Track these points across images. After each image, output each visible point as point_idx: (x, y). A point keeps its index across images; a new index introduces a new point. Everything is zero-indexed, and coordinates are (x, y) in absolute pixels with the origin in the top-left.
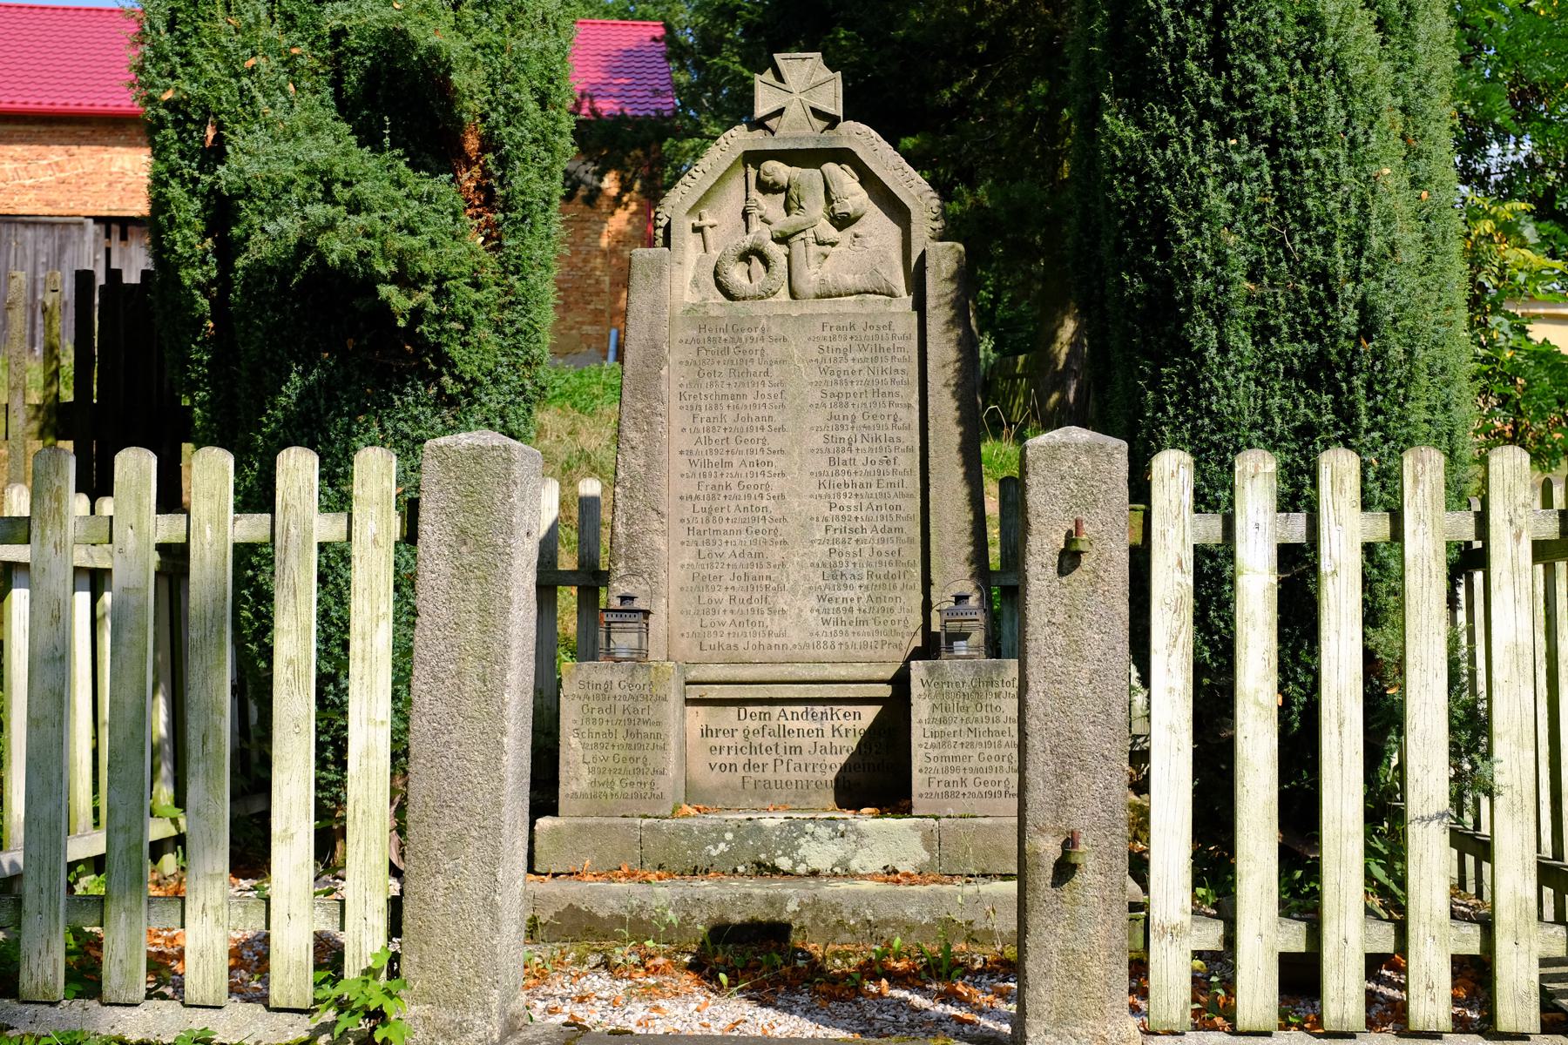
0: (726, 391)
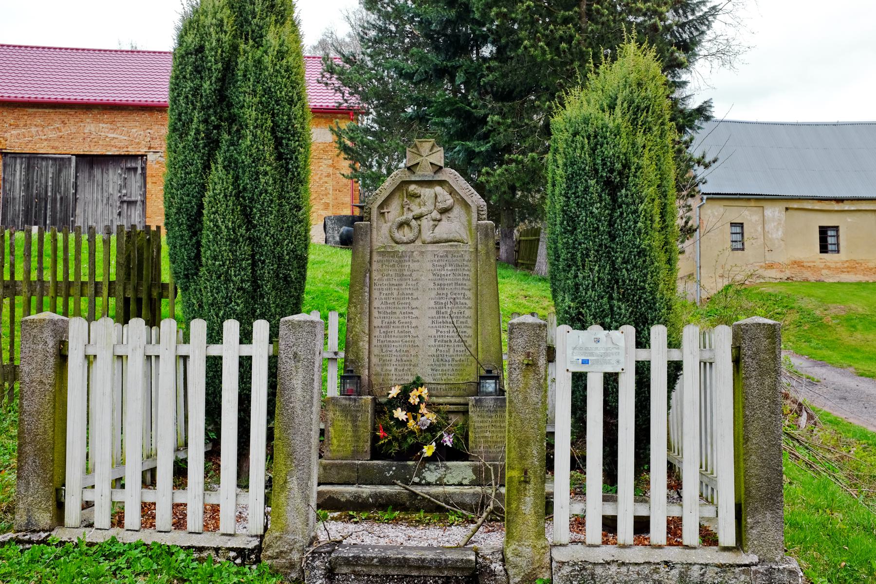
0: (394, 282)
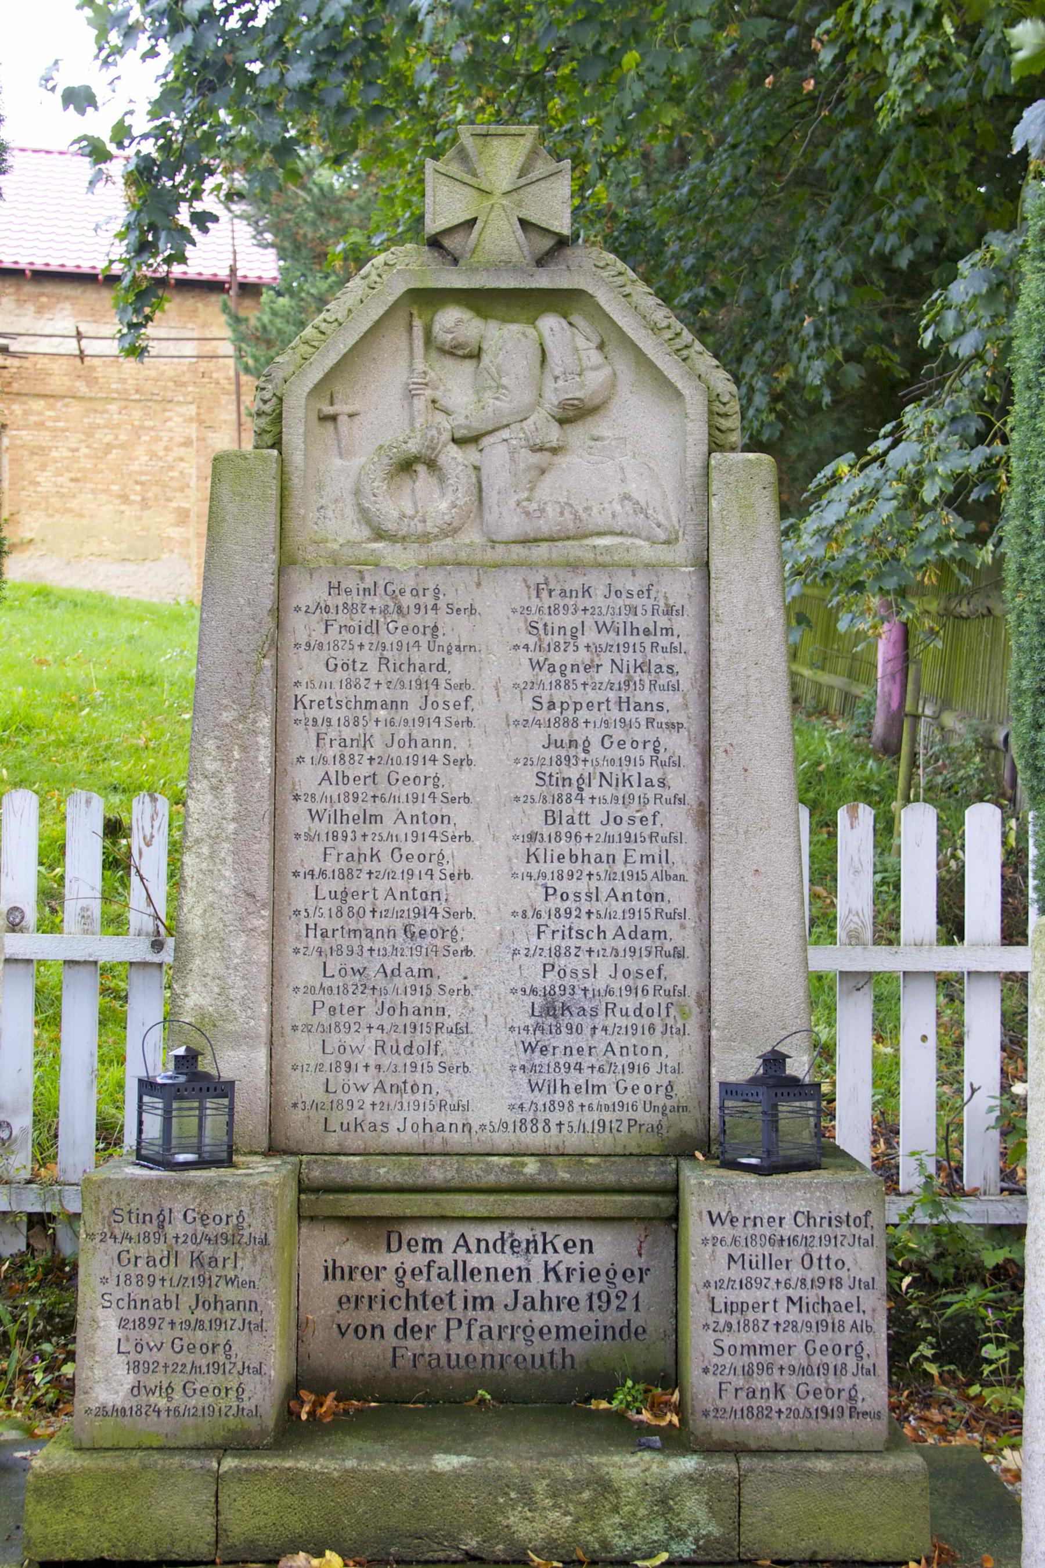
0: (372, 694)
